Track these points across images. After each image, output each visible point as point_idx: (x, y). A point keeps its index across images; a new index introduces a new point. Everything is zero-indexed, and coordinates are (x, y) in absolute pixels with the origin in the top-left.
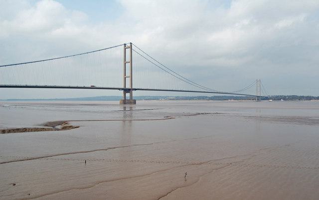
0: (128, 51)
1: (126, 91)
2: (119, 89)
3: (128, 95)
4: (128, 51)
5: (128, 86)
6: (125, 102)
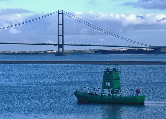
1: (60, 46)
3: (61, 49)
5: (61, 43)
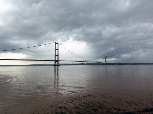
0: (57, 45)
2: (53, 61)
3: (56, 63)
4: (57, 45)
5: (57, 59)
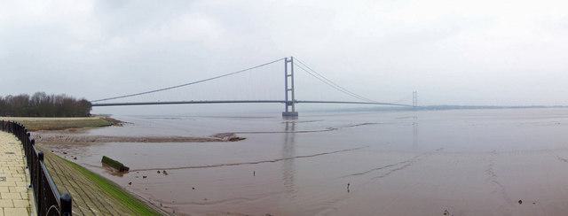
0: (289, 64)
1: (288, 103)
4: (289, 64)
5: (290, 99)
6: (286, 115)
